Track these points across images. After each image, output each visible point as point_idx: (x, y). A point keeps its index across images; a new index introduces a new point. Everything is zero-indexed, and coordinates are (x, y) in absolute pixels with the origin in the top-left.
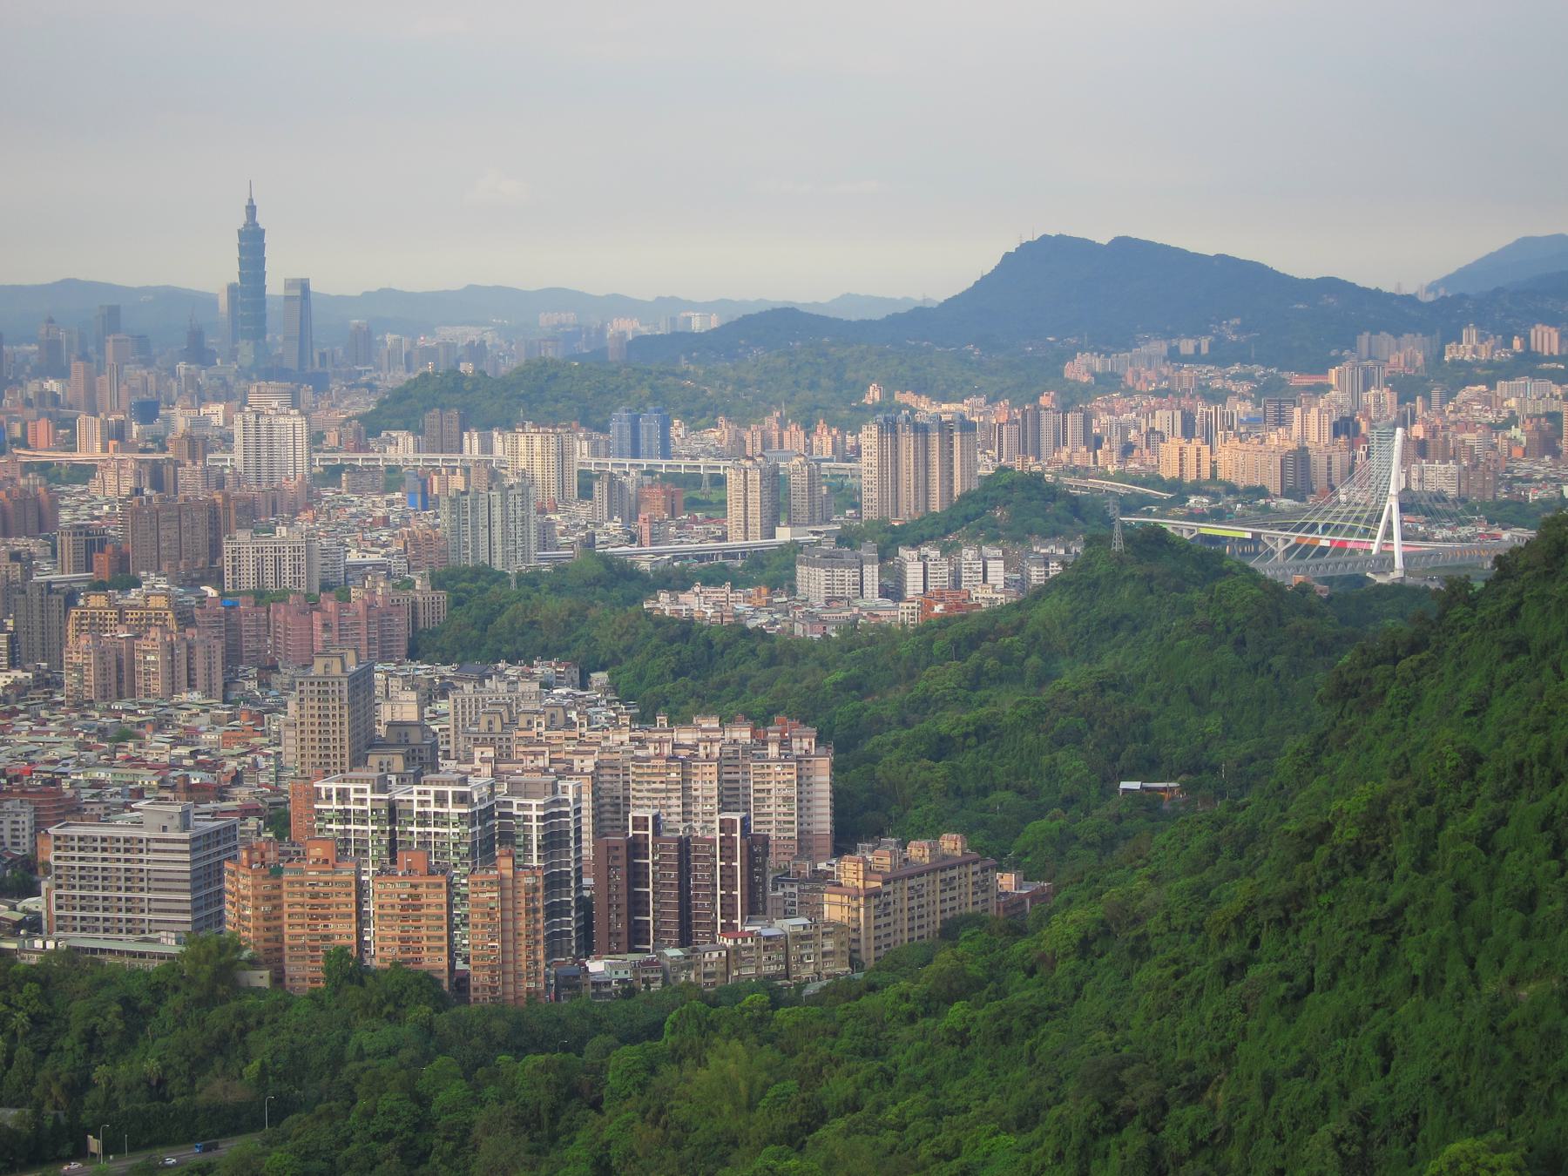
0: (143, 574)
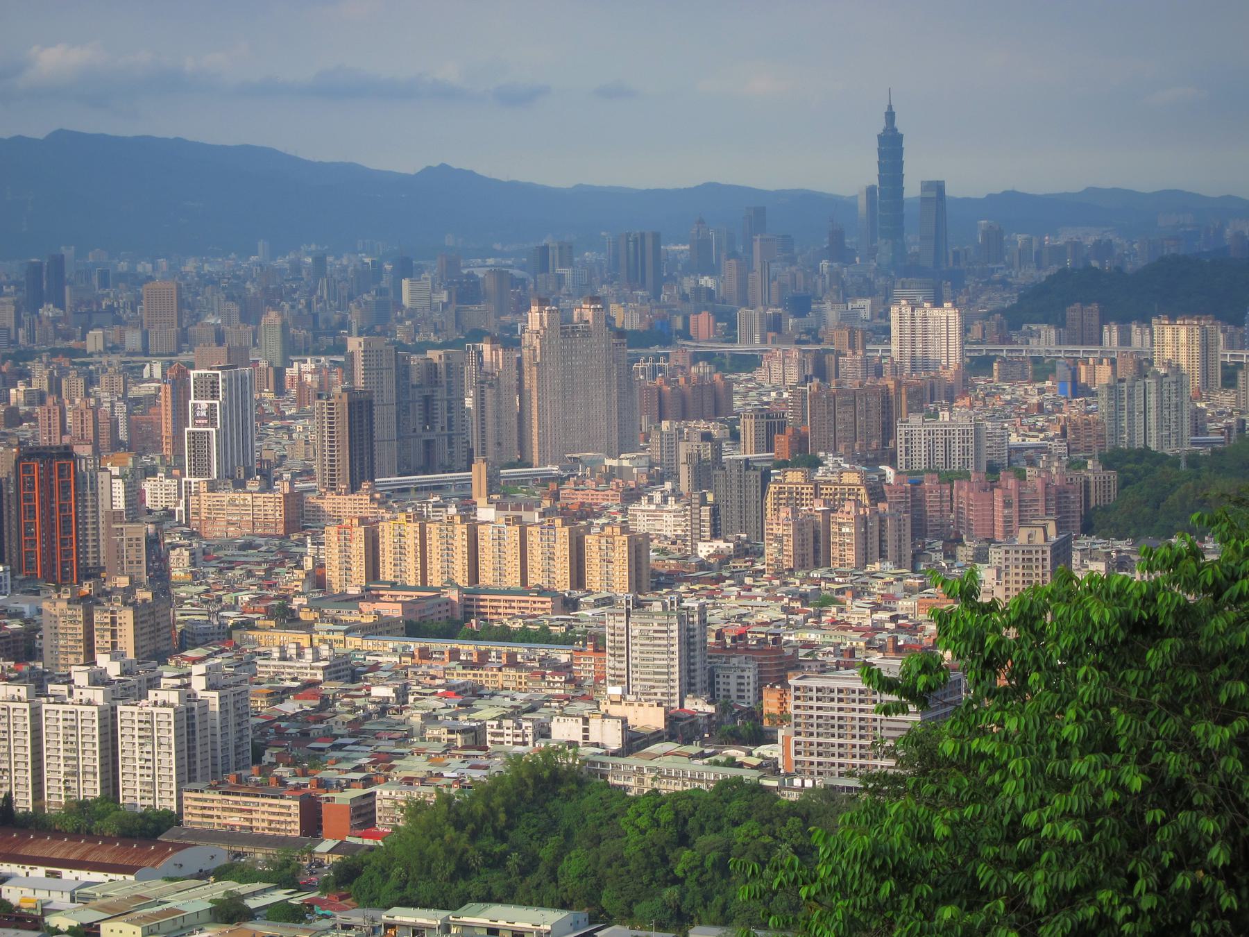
0: (822, 454)
